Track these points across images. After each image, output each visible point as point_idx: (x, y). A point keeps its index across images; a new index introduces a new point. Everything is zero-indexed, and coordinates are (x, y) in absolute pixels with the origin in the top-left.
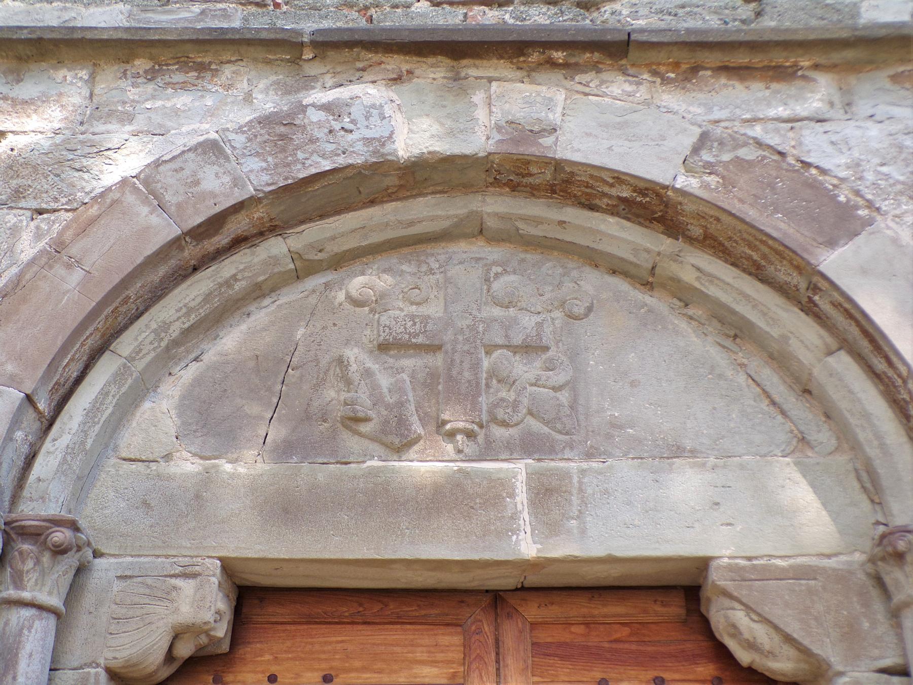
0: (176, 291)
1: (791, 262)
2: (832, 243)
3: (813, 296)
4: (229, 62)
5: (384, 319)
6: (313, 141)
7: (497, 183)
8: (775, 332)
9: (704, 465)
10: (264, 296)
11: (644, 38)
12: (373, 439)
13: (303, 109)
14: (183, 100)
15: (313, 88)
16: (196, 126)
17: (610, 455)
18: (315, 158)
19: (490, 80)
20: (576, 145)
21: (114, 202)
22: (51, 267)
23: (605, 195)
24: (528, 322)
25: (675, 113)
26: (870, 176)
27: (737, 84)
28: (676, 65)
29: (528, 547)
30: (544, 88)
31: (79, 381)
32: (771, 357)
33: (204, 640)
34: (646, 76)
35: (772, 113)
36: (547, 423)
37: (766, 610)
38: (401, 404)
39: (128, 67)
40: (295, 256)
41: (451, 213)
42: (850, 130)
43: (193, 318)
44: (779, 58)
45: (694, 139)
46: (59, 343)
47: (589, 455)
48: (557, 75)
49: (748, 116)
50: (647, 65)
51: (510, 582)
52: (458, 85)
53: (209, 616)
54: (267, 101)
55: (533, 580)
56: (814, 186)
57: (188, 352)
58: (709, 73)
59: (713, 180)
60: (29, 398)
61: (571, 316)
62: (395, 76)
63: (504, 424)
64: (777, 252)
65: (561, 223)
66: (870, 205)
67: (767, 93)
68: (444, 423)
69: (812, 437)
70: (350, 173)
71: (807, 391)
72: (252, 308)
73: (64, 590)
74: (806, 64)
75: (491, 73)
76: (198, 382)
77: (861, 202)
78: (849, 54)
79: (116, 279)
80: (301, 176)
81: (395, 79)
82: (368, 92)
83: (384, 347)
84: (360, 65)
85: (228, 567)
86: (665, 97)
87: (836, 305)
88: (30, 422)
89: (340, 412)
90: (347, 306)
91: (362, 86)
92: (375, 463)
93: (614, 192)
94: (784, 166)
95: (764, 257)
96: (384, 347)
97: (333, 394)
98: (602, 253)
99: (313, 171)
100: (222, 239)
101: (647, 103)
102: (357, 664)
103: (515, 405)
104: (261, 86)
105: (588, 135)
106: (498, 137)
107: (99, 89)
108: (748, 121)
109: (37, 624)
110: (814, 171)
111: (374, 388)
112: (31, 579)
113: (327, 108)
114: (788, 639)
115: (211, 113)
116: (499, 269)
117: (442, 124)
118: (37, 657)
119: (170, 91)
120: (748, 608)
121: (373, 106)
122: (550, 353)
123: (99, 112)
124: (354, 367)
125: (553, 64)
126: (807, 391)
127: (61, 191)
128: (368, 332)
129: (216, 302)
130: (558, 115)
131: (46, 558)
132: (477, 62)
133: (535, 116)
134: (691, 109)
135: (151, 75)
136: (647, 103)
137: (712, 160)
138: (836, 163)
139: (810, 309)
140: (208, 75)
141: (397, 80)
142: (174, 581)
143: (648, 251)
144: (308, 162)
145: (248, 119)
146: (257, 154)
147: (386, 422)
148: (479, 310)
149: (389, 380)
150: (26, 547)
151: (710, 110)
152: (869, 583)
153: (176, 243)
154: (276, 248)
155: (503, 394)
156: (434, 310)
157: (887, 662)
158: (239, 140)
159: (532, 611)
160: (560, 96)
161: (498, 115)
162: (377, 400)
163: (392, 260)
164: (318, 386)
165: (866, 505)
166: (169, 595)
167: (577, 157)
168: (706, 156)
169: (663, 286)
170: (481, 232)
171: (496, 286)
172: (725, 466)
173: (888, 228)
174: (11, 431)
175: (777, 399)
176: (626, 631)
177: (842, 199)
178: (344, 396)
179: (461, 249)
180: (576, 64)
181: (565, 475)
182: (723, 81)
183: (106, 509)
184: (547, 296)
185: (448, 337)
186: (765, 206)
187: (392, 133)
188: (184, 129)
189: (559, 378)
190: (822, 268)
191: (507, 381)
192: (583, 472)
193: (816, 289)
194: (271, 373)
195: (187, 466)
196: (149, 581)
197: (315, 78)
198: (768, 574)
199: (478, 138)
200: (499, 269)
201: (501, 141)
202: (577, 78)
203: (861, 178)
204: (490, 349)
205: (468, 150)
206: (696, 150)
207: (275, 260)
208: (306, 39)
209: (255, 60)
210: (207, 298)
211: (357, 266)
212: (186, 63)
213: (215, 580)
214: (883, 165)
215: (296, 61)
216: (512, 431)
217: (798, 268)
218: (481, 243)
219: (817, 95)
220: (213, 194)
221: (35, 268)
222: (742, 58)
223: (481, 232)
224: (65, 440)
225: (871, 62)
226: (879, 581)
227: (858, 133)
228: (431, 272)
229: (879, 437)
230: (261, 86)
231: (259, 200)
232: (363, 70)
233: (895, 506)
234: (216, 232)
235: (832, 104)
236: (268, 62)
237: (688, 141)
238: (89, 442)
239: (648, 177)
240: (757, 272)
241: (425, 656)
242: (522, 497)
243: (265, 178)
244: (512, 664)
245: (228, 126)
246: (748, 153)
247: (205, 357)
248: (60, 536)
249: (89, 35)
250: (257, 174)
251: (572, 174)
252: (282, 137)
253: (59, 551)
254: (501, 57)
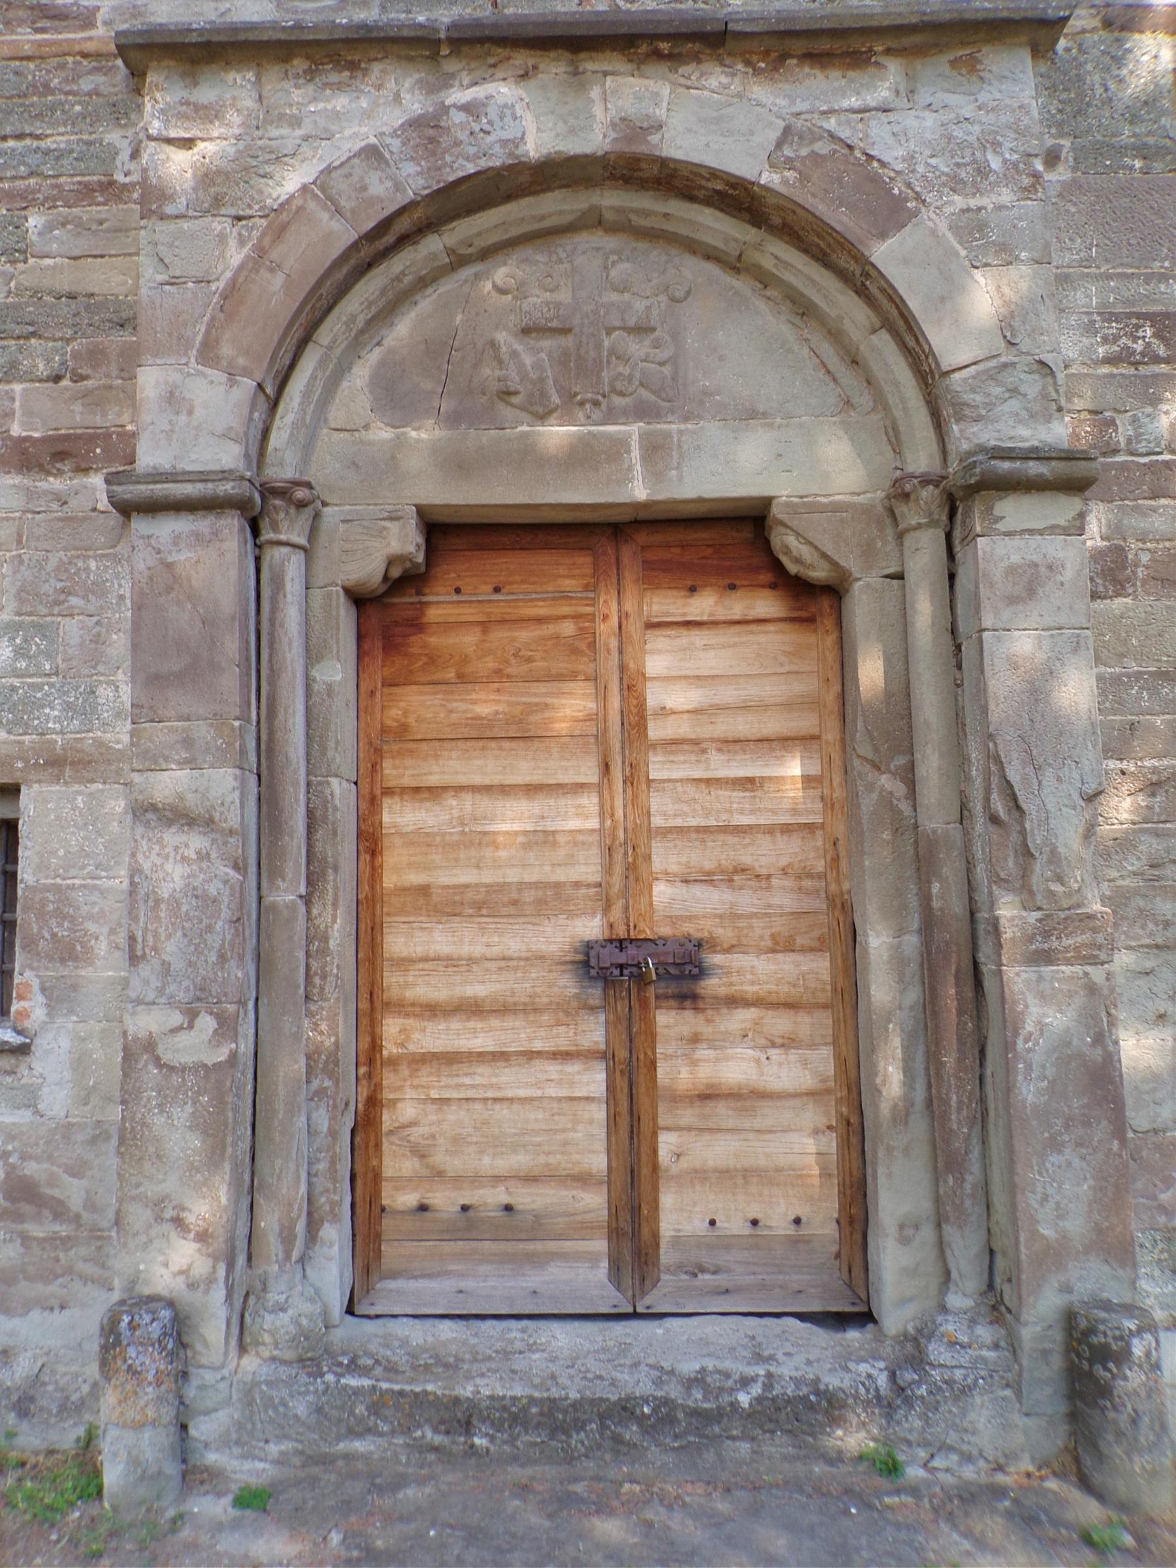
0: (358, 286)
1: (849, 252)
2: (883, 235)
3: (864, 281)
4: (376, 59)
5: (525, 305)
6: (457, 143)
7: (612, 177)
8: (833, 313)
9: (771, 425)
10: (426, 286)
11: (738, 27)
12: (521, 408)
13: (445, 109)
14: (341, 102)
15: (452, 86)
16: (356, 129)
17: (700, 417)
18: (461, 161)
19: (606, 74)
20: (679, 142)
21: (300, 209)
22: (258, 272)
23: (701, 187)
24: (640, 305)
25: (764, 106)
26: (921, 169)
27: (817, 72)
28: (767, 53)
29: (639, 491)
30: (652, 82)
31: (292, 366)
32: (829, 332)
33: (408, 565)
34: (740, 66)
35: (846, 104)
36: (654, 392)
37: (810, 535)
38: (542, 380)
39: (288, 66)
40: (450, 251)
41: (575, 207)
42: (909, 120)
43: (374, 310)
44: (856, 44)
45: (778, 133)
46: (276, 339)
47: (686, 419)
48: (662, 68)
49: (825, 108)
50: (742, 54)
51: (627, 518)
52: (577, 80)
53: (412, 549)
54: (415, 104)
55: (642, 515)
56: (875, 179)
57: (371, 338)
58: (795, 61)
59: (791, 175)
60: (260, 386)
61: (673, 300)
62: (521, 72)
63: (621, 394)
64: (839, 243)
65: (666, 215)
66: (918, 197)
67: (843, 82)
68: (576, 394)
69: (855, 400)
70: (490, 174)
71: (855, 362)
72: (418, 297)
73: (307, 533)
74: (879, 49)
75: (606, 67)
76: (382, 363)
77: (911, 194)
78: (917, 39)
79: (312, 281)
80: (451, 178)
81: (522, 76)
82: (502, 91)
83: (526, 331)
84: (491, 60)
85: (421, 511)
86: (756, 88)
87: (883, 290)
88: (262, 405)
89: (495, 387)
90: (495, 294)
91: (495, 84)
92: (525, 428)
93: (710, 185)
94: (852, 160)
95: (829, 246)
96: (526, 331)
97: (488, 371)
98: (699, 242)
99: (461, 174)
100: (389, 239)
101: (739, 96)
102: (518, 578)
103: (630, 378)
104: (407, 85)
105: (689, 130)
106: (613, 135)
107: (267, 88)
108: (824, 113)
109: (293, 558)
110: (875, 164)
111: (521, 366)
112: (284, 526)
113: (466, 108)
114: (824, 556)
115: (367, 115)
116: (616, 258)
117: (565, 122)
118: (297, 581)
119: (328, 92)
120: (798, 534)
121: (506, 106)
122: (657, 333)
123: (270, 116)
124: (504, 349)
125: (658, 55)
126: (855, 362)
127: (252, 199)
128: (512, 317)
129: (390, 295)
130: (664, 110)
131: (292, 510)
132: (594, 55)
133: (644, 112)
134: (778, 101)
135: (310, 75)
136: (739, 96)
137: (792, 155)
138: (893, 154)
139: (862, 292)
140: (359, 74)
141: (524, 76)
142: (383, 523)
143: (736, 240)
144: (456, 165)
145: (400, 122)
146: (412, 159)
147: (532, 394)
148: (600, 296)
149: (531, 358)
150: (278, 502)
151: (793, 102)
152: (885, 514)
153: (355, 246)
154: (433, 245)
155: (620, 369)
156: (564, 296)
157: (891, 571)
158: (396, 144)
159: (643, 538)
160: (666, 91)
161: (613, 112)
162: (524, 377)
163: (527, 251)
164: (476, 366)
165: (890, 454)
166: (381, 533)
167: (679, 155)
168: (788, 151)
169: (747, 270)
170: (600, 223)
171: (613, 273)
172: (788, 425)
173: (929, 219)
174: (251, 413)
175: (831, 367)
176: (710, 550)
177: (896, 191)
178: (497, 373)
179: (587, 240)
180: (680, 54)
181: (667, 435)
182: (807, 70)
183: (325, 469)
184: (655, 282)
185: (576, 321)
186: (833, 200)
187: (524, 134)
188: (347, 133)
189: (665, 354)
190: (873, 259)
191: (623, 358)
192: (681, 432)
193: (867, 275)
194: (438, 351)
195: (383, 433)
196: (366, 523)
197: (452, 76)
198: (814, 508)
199: (595, 140)
200: (616, 258)
201: (615, 140)
202: (680, 71)
203: (913, 171)
204: (609, 331)
205: (588, 149)
206: (779, 145)
207: (433, 256)
208: (442, 35)
209: (399, 57)
210: (383, 292)
211: (500, 258)
212: (338, 62)
213: (413, 522)
214: (932, 156)
215: (434, 57)
216: (628, 400)
217: (855, 258)
218: (600, 233)
219: (883, 84)
220: (379, 199)
221: (245, 273)
222: (825, 45)
223: (600, 223)
224: (290, 418)
225: (936, 45)
226: (891, 512)
227: (916, 123)
228: (560, 261)
229: (903, 401)
230: (407, 85)
231: (418, 203)
232: (494, 66)
233: (909, 456)
234: (384, 234)
235: (897, 92)
236: (411, 59)
237: (774, 135)
238: (308, 418)
239: (738, 173)
240: (823, 259)
241: (566, 572)
242: (636, 453)
243: (421, 182)
244: (629, 577)
245: (384, 129)
246: (822, 148)
247: (385, 342)
248: (300, 494)
249: (251, 36)
250: (412, 179)
251: (675, 170)
252: (432, 140)
253: (301, 505)
254: (614, 50)
